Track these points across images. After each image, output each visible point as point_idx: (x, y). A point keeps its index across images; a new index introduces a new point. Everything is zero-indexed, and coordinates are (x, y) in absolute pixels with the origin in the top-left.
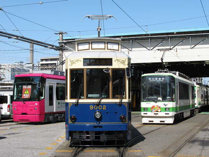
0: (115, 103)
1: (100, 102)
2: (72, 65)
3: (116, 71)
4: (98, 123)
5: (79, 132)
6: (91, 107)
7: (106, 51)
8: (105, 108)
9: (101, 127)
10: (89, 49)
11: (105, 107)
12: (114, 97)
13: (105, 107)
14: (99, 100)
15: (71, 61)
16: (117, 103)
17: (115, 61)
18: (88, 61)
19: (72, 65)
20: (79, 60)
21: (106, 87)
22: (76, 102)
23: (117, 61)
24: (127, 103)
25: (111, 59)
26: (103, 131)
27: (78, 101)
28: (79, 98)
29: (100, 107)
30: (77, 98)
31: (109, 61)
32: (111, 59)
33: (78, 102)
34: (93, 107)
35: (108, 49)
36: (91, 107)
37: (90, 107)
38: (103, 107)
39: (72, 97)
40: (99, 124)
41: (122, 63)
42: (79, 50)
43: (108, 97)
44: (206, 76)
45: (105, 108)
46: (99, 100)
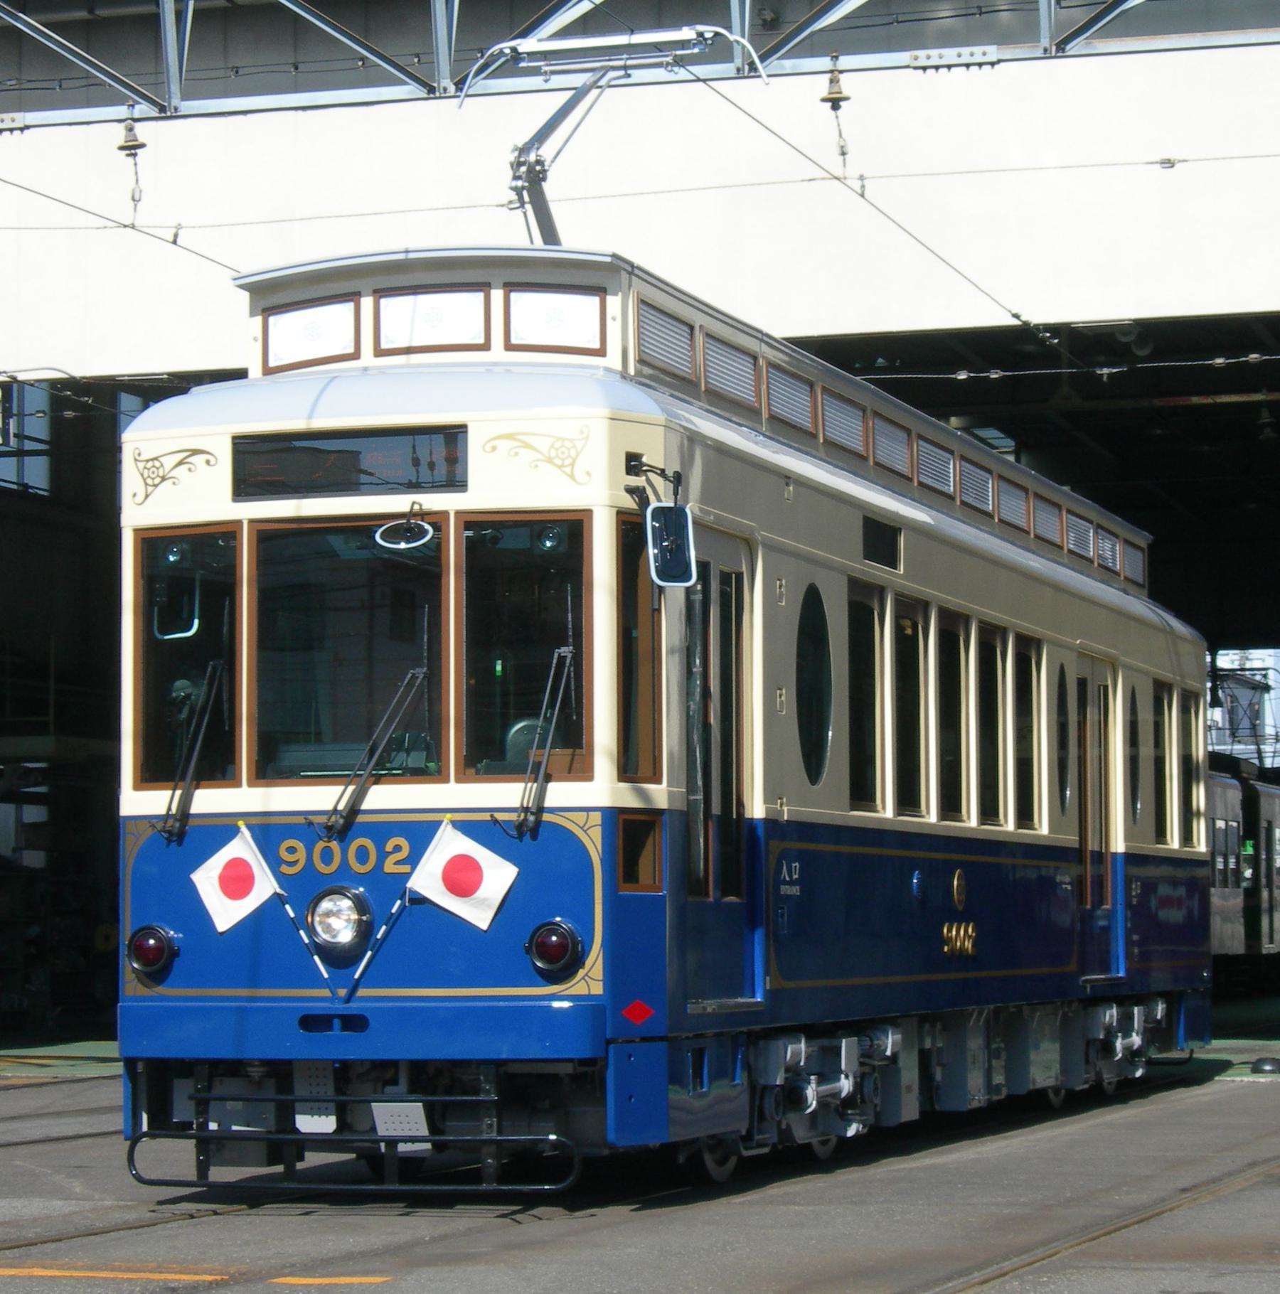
0: (301, 820)
1: (354, 809)
2: (147, 496)
3: (492, 537)
4: (343, 992)
5: (267, 1075)
6: (292, 850)
7: (366, 369)
8: (397, 863)
9: (355, 1023)
10: (486, 347)
11: (398, 848)
12: (270, 769)
13: (398, 848)
14: (351, 788)
15: (141, 465)
16: (500, 816)
17: (494, 448)
18: (264, 462)
19: (147, 496)
20: (195, 452)
21: (414, 677)
22: (335, 811)
23: (504, 445)
24: (596, 818)
25: (453, 436)
26: (394, 1064)
27: (186, 801)
28: (193, 779)
29: (362, 855)
30: (183, 778)
31: (438, 452)
32: (453, 436)
33: (184, 812)
34: (301, 855)
35: (379, 352)
36: (292, 850)
37: (321, 845)
38: (389, 847)
39: (150, 776)
40: (349, 998)
41: (550, 460)
42: (272, 363)
43: (430, 772)
44: (336, 542)
45: (397, 863)
46: (351, 788)
